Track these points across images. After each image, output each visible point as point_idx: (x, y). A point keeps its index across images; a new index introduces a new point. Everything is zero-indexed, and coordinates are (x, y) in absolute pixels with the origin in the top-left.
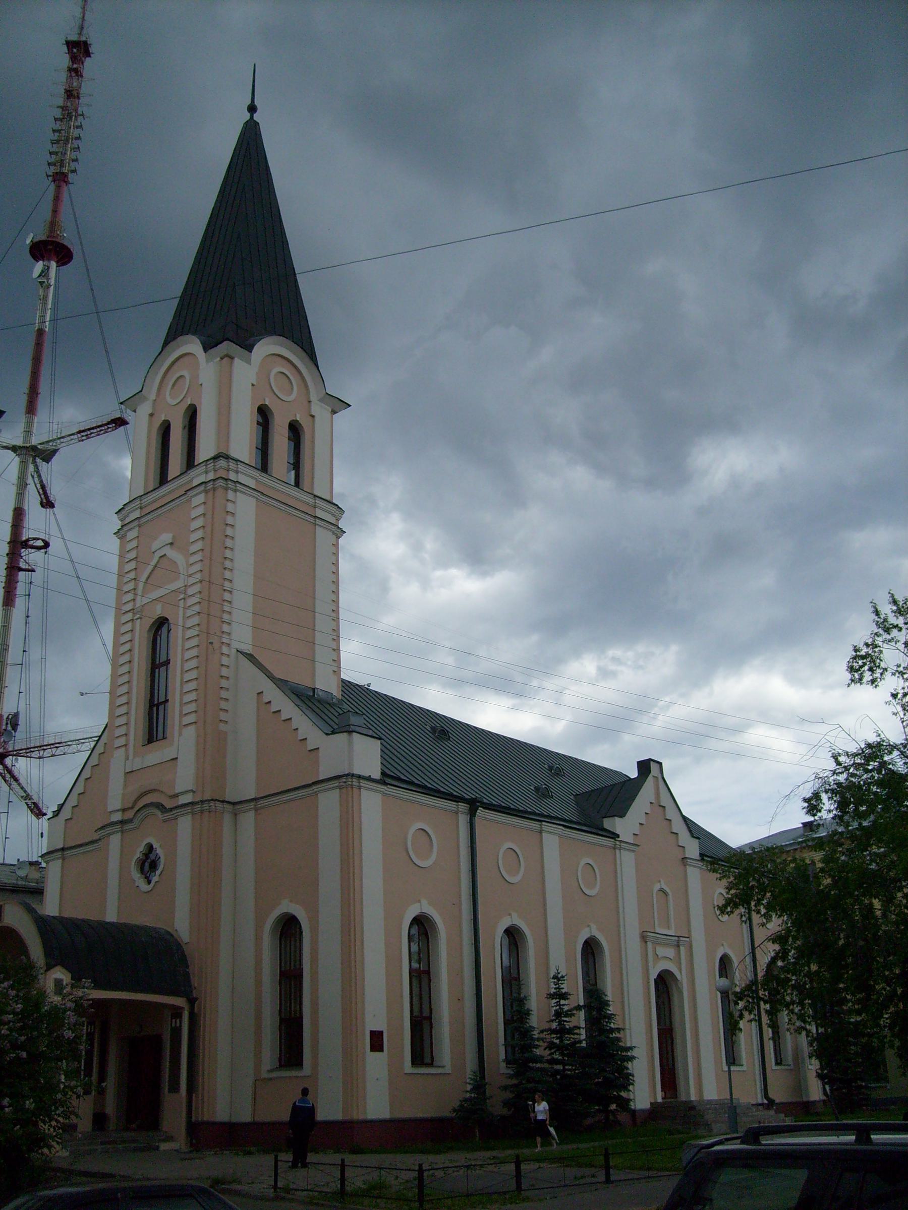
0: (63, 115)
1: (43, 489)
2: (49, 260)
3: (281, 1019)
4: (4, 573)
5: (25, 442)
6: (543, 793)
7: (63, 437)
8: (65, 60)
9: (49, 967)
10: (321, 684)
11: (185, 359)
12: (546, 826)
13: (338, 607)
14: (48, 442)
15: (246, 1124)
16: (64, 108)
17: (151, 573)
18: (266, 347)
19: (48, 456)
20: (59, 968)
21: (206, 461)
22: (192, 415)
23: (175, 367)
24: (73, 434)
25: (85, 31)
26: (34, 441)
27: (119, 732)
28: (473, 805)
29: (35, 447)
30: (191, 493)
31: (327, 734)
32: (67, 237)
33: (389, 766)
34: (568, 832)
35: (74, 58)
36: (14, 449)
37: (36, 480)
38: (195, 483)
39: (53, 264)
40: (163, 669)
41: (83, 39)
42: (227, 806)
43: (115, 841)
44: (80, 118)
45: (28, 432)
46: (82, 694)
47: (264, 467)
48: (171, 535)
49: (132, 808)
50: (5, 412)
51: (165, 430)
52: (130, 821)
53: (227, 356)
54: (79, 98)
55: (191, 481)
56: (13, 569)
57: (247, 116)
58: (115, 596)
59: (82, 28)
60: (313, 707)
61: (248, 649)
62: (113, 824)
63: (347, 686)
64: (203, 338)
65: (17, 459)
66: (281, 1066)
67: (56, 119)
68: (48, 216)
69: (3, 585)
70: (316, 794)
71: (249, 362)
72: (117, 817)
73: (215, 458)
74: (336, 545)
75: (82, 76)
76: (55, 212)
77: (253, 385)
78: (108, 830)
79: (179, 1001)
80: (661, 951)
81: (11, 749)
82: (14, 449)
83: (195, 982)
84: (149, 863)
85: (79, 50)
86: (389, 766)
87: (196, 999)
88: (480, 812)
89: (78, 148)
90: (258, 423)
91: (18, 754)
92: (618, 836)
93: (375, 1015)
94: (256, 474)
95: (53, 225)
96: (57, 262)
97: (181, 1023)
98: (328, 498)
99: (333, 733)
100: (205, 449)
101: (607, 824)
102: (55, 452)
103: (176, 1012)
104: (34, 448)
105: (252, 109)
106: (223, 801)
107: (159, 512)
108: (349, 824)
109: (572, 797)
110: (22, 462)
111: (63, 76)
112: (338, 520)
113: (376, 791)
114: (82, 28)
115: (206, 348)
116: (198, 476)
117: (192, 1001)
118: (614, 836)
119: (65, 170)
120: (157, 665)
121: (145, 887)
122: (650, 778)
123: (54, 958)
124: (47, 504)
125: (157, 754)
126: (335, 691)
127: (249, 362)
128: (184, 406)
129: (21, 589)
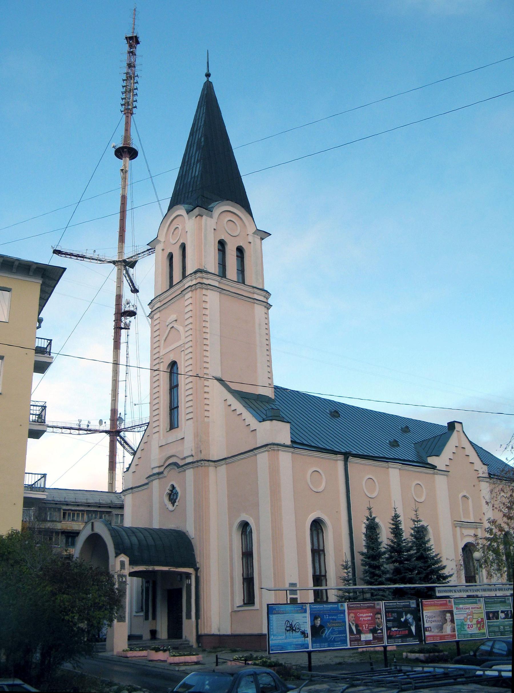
0: (127, 77)
1: (132, 283)
3: (244, 579)
4: (113, 331)
6: (395, 444)
7: (139, 254)
8: (126, 48)
10: (261, 391)
11: (178, 218)
12: (391, 464)
13: (270, 349)
14: (132, 257)
15: (228, 636)
16: (127, 73)
17: (166, 338)
19: (132, 265)
20: (122, 555)
21: (191, 274)
22: (183, 247)
24: (145, 252)
25: (135, 31)
26: (125, 257)
27: (155, 424)
28: (347, 456)
29: (125, 260)
30: (184, 293)
31: (260, 422)
32: (135, 144)
33: (297, 435)
34: (405, 467)
35: (131, 46)
36: (114, 262)
37: (128, 278)
38: (186, 286)
39: (128, 159)
40: (175, 389)
43: (156, 484)
44: (136, 78)
45: (121, 252)
47: (223, 274)
48: (175, 316)
49: (163, 466)
50: (65, 269)
51: (171, 257)
52: (162, 473)
53: (199, 215)
54: (135, 67)
56: (118, 329)
57: (205, 79)
58: (111, 369)
60: (252, 406)
61: (219, 375)
62: (154, 475)
64: (186, 206)
65: (116, 268)
66: (244, 604)
68: (123, 133)
69: (113, 338)
70: (256, 455)
71: (211, 217)
72: (156, 471)
73: (195, 272)
74: (267, 314)
75: (135, 55)
76: (127, 130)
77: (214, 229)
78: (152, 478)
79: (190, 570)
80: (466, 532)
81: (123, 427)
82: (114, 262)
83: (198, 559)
85: (133, 41)
86: (297, 435)
87: (198, 569)
89: (137, 94)
90: (219, 250)
91: (126, 430)
92: (436, 467)
94: (219, 279)
95: (127, 137)
96: (130, 158)
97: (191, 581)
98: (260, 287)
99: (264, 420)
101: (431, 460)
102: (136, 262)
103: (188, 576)
104: (124, 261)
105: (208, 75)
106: (208, 461)
109: (413, 445)
111: (126, 56)
112: (267, 299)
113: (288, 452)
115: (188, 212)
116: (188, 283)
117: (197, 570)
118: (434, 467)
119: (130, 107)
120: (173, 388)
122: (455, 432)
123: (120, 549)
124: (135, 291)
125: (176, 434)
126: (270, 393)
128: (179, 244)
129: (123, 338)
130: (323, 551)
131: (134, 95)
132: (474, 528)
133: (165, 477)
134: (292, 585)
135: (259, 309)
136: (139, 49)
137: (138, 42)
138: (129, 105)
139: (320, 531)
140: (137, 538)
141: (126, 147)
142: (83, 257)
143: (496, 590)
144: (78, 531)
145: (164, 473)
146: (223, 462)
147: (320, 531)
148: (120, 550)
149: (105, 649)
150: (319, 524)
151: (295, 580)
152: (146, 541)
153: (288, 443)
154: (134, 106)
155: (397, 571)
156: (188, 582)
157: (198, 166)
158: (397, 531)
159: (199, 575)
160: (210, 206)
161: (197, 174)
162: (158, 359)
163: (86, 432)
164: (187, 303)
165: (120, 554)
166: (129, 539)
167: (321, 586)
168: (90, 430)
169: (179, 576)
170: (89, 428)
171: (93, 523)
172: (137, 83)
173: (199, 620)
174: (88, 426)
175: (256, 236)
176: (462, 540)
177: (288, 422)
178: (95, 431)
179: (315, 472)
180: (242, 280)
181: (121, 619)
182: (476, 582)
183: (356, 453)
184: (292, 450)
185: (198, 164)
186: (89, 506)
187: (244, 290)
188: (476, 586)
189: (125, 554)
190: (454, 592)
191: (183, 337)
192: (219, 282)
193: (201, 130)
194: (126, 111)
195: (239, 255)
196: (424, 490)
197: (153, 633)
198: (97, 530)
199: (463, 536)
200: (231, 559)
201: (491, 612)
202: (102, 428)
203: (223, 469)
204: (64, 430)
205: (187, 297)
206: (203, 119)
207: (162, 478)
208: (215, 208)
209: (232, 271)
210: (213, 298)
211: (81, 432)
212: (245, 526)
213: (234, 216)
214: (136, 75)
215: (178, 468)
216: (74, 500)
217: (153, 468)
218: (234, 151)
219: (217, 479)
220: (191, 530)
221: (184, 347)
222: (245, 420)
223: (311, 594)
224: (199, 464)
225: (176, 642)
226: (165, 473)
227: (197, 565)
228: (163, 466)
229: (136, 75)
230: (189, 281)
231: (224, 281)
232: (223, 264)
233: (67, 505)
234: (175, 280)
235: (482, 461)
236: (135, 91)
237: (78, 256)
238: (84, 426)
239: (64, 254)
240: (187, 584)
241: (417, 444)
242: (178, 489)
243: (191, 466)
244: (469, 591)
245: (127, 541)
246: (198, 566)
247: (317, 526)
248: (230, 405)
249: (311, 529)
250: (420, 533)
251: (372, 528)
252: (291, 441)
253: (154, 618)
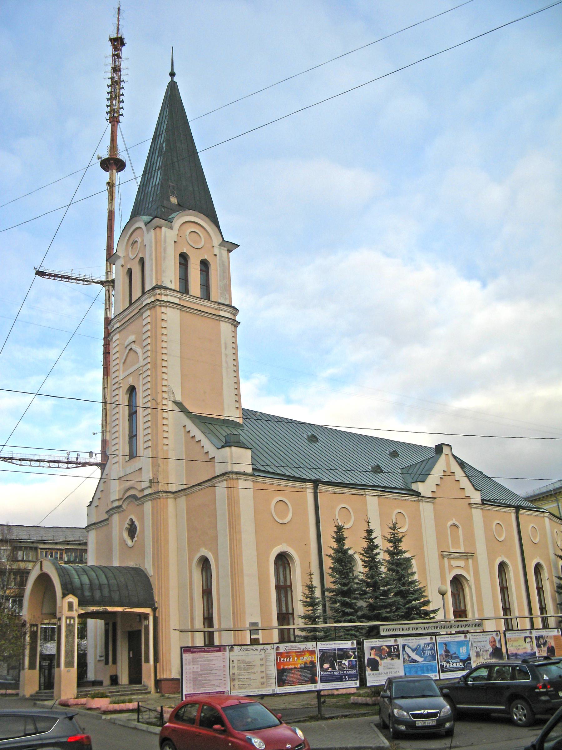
0: (112, 82)
2: (112, 169)
5: (107, 278)
6: (377, 470)
8: (110, 50)
9: (64, 595)
12: (368, 492)
16: (111, 78)
17: (125, 360)
20: (70, 596)
22: (142, 262)
25: (120, 31)
28: (316, 483)
30: (142, 311)
32: (122, 156)
34: (386, 494)
35: (115, 48)
36: (102, 283)
38: (144, 304)
39: (114, 171)
40: (134, 416)
41: (119, 36)
42: (169, 495)
43: (116, 518)
44: (122, 84)
47: (185, 289)
49: (122, 499)
51: (130, 273)
52: (120, 507)
53: (158, 227)
54: (120, 71)
55: (142, 303)
59: (118, 29)
62: (113, 508)
63: (248, 414)
67: (108, 86)
68: (109, 143)
69: (102, 363)
71: (171, 228)
72: (116, 504)
73: (154, 289)
74: (234, 332)
75: (121, 58)
77: (175, 242)
78: (111, 512)
80: (455, 563)
82: (102, 283)
84: (132, 531)
85: (118, 43)
87: (156, 608)
88: (321, 486)
92: (420, 494)
93: (252, 615)
94: (179, 295)
95: (113, 147)
103: (146, 616)
105: (172, 74)
107: (131, 321)
108: (233, 503)
110: (106, 290)
111: (110, 60)
112: (235, 316)
114: (118, 29)
117: (154, 610)
119: (116, 115)
121: (130, 543)
123: (68, 589)
125: (136, 464)
127: (171, 228)
128: (137, 259)
130: (290, 587)
131: (120, 102)
132: (465, 559)
133: (124, 510)
134: (253, 624)
135: (225, 327)
136: (125, 52)
137: (123, 44)
138: (115, 112)
139: (287, 565)
140: (88, 577)
141: (112, 159)
142: (68, 278)
143: (451, 627)
145: (123, 506)
146: (182, 493)
147: (287, 565)
148: (67, 590)
149: (52, 696)
150: (286, 558)
151: (257, 619)
152: (98, 579)
153: (249, 470)
154: (121, 113)
155: (371, 607)
156: (146, 623)
157: (159, 174)
158: (372, 564)
159: (157, 615)
160: (170, 217)
161: (157, 183)
162: (117, 384)
163: (75, 465)
164: (145, 323)
165: (68, 594)
166: (79, 578)
167: (289, 625)
168: (80, 463)
169: (138, 617)
170: (79, 461)
171: (41, 562)
172: (123, 88)
173: (158, 664)
174: (77, 458)
175: (222, 248)
176: (450, 572)
177: (248, 448)
178: (85, 464)
179: (280, 502)
180: (206, 294)
182: (466, 617)
183: (335, 481)
184: (253, 478)
185: (159, 172)
186: (68, 544)
187: (210, 307)
188: (466, 621)
189: (74, 595)
190: (401, 630)
191: (141, 359)
192: (179, 299)
193: (163, 135)
194: (112, 120)
195: (204, 268)
196: (407, 520)
197: (114, 680)
198: (45, 570)
199: (451, 567)
200: (192, 598)
202: (92, 461)
203: (182, 501)
204: (51, 464)
205: (145, 315)
206: (166, 123)
207: (121, 512)
208: (175, 219)
209: (195, 287)
210: (172, 316)
211: (70, 465)
212: (205, 563)
213: (198, 227)
214: (122, 80)
215: (136, 500)
216: (51, 538)
217: (113, 502)
218: (203, 157)
219: (174, 512)
220: (149, 568)
221: (142, 370)
222: (203, 447)
223: (276, 633)
224: (157, 496)
225: (137, 687)
226: (124, 507)
227: (156, 604)
228: (122, 499)
229: (122, 80)
230: (147, 299)
231: (185, 297)
232: (184, 280)
233: (45, 543)
235: (473, 486)
236: (121, 97)
237: (62, 277)
238: (73, 458)
239: (48, 275)
240: (145, 626)
241: (399, 469)
242: (137, 523)
243: (149, 498)
244: (411, 629)
245: (76, 580)
246: (156, 605)
247: (283, 560)
248: (189, 432)
249: (276, 563)
250: (400, 565)
251: (343, 560)
252: (253, 469)
253: (115, 662)
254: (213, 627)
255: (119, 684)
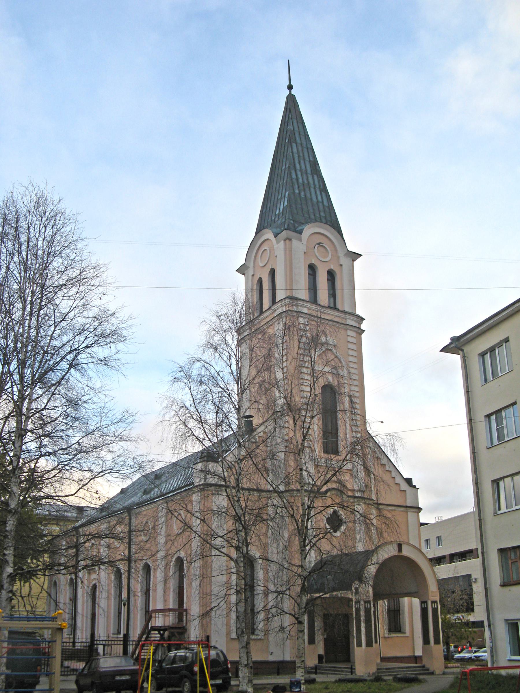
6: (196, 460)
11: (266, 242)
18: (308, 230)
22: (273, 273)
23: (262, 246)
46: (382, 422)
47: (314, 300)
57: (288, 92)
71: (300, 240)
77: (304, 253)
100: (280, 295)
105: (290, 87)
127: (300, 240)
144: (402, 630)
181: (12, 672)
192: (309, 309)
201: (62, 662)
209: (323, 297)
234: (266, 307)
254: (482, 622)
255: (435, 675)
